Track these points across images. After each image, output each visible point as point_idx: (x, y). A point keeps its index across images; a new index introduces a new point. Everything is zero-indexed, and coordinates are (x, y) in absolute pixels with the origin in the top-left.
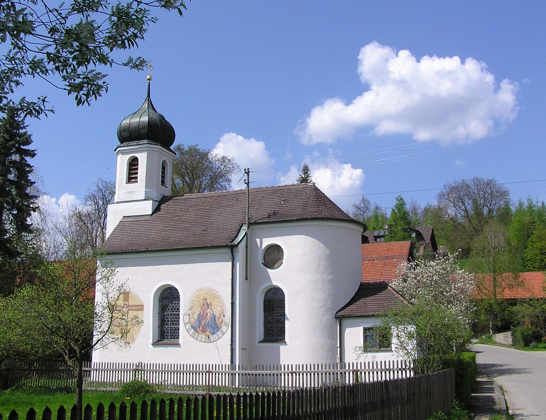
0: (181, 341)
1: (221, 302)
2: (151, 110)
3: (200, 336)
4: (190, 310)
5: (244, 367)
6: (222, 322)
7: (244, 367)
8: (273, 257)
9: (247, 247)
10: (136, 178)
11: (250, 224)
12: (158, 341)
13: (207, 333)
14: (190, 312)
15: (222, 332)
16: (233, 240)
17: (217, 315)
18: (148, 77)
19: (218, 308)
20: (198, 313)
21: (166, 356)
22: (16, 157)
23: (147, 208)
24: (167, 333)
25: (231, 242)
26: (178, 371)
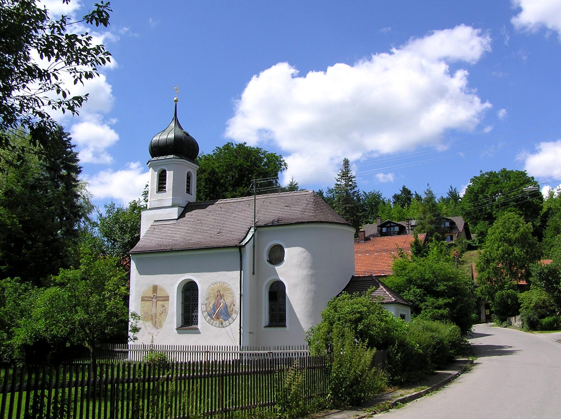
0: (199, 326)
1: (232, 293)
2: (178, 128)
3: (215, 322)
4: (206, 300)
5: (252, 348)
6: (232, 311)
7: (252, 348)
8: (276, 255)
9: (254, 246)
10: (165, 188)
11: (257, 227)
12: (182, 326)
13: (221, 320)
14: (207, 302)
15: (233, 318)
16: (242, 241)
17: (229, 305)
18: (175, 99)
19: (230, 299)
20: (213, 303)
21: (188, 340)
22: (64, 172)
23: (174, 213)
24: (188, 320)
25: (240, 243)
26: (196, 351)
